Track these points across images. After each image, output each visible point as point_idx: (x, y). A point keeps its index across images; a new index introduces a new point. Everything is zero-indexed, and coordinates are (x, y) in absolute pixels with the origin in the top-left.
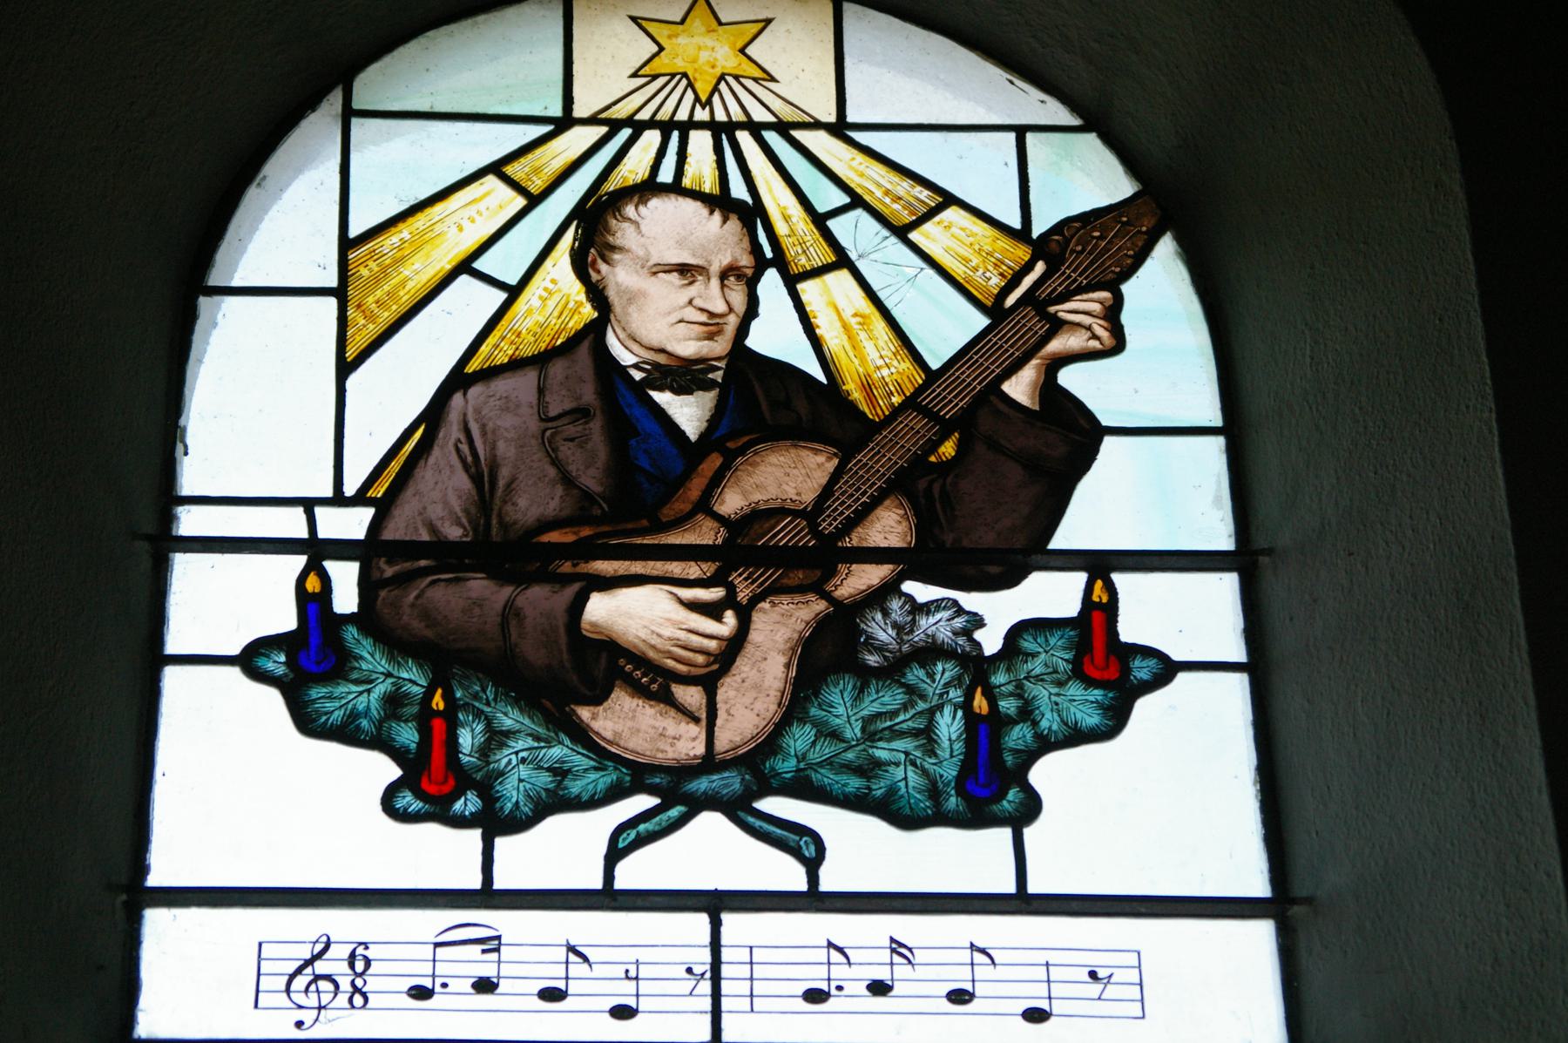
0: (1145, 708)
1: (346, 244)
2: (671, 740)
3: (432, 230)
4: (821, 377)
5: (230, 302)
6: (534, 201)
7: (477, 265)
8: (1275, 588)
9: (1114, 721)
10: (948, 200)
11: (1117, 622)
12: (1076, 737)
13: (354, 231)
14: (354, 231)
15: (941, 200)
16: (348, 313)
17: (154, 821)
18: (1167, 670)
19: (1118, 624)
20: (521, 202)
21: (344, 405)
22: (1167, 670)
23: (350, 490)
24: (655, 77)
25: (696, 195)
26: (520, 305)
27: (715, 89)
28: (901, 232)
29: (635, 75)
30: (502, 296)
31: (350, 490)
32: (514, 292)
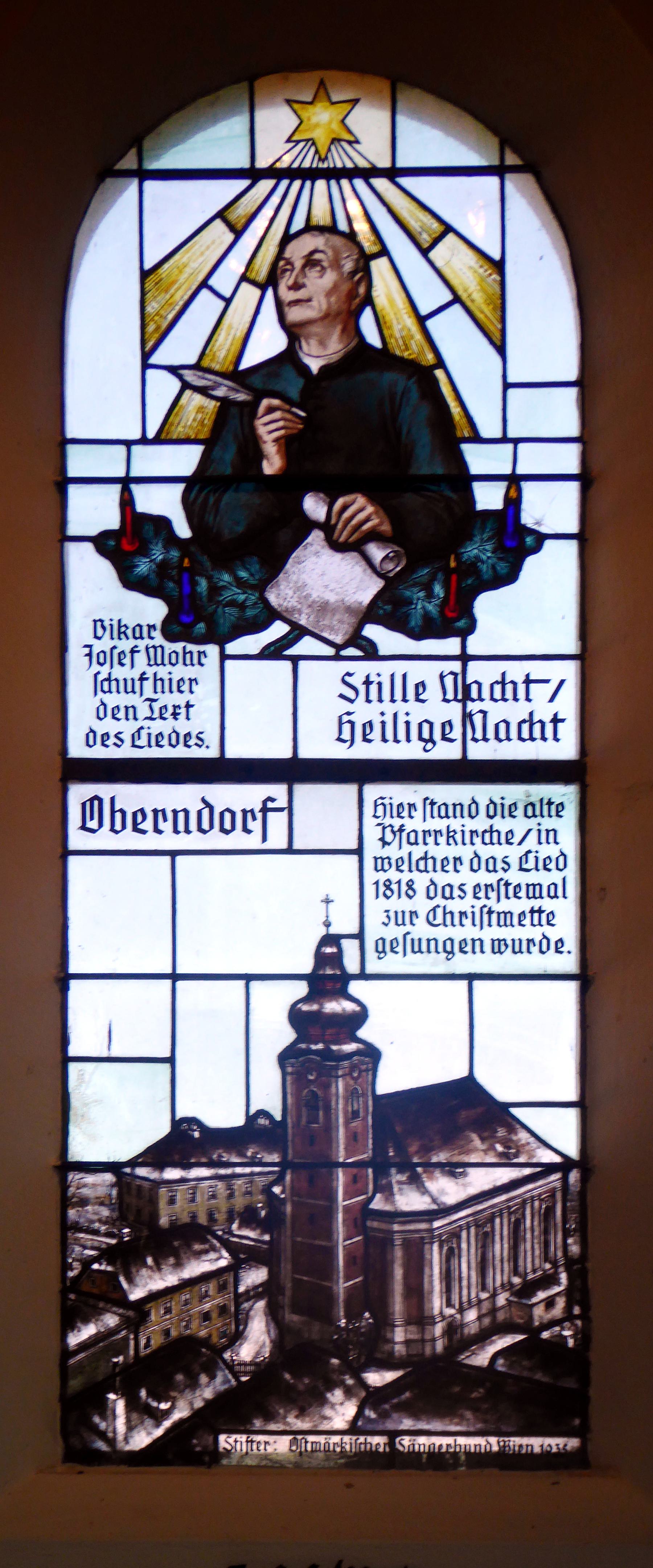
0: (531, 563)
1: (145, 275)
6: (238, 233)
24: (298, 142)
27: (329, 150)
29: (289, 140)
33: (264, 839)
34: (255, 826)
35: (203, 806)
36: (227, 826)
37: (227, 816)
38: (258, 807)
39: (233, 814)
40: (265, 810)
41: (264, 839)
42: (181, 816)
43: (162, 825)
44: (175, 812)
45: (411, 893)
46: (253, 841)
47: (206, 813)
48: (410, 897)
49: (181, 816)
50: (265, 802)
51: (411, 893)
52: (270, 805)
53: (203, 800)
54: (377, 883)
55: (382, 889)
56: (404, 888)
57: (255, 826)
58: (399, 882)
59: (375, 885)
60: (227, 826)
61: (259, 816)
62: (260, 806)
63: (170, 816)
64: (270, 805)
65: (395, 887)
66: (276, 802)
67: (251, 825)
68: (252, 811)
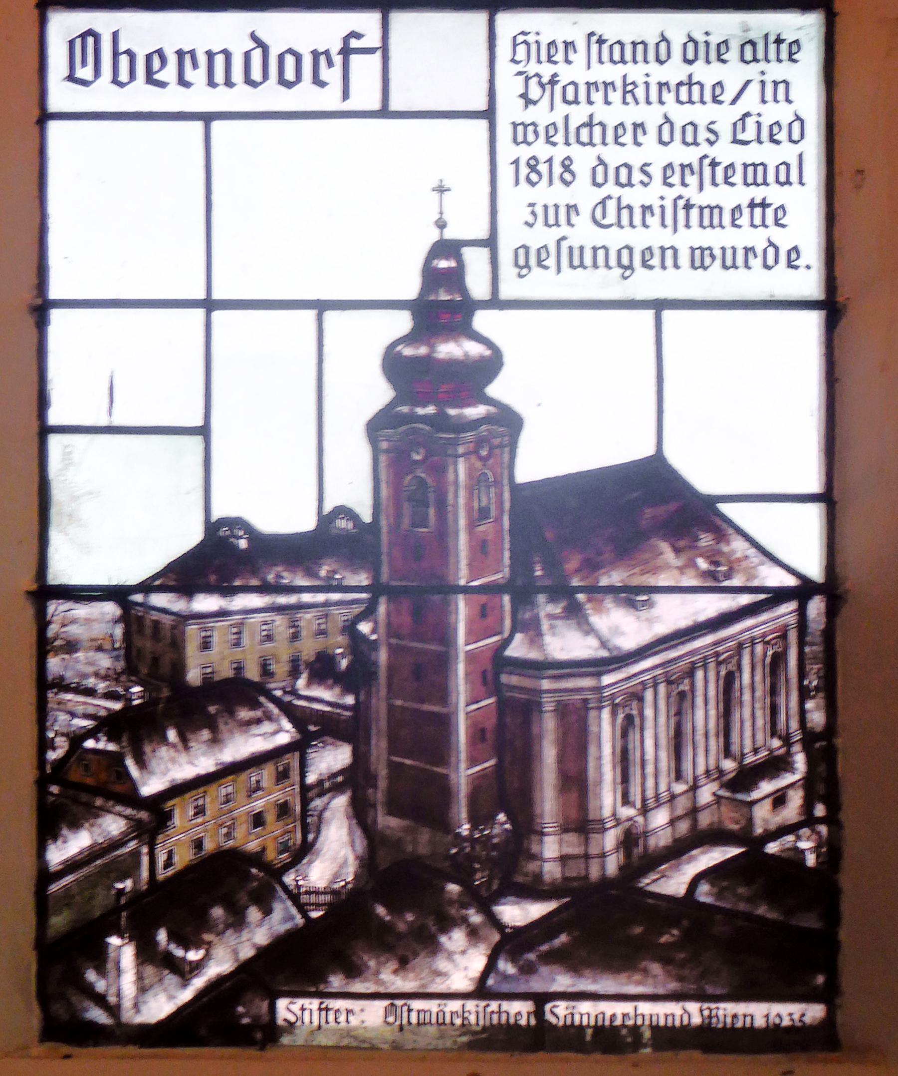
33: (346, 95)
34: (332, 75)
35: (254, 45)
36: (290, 75)
37: (290, 60)
38: (335, 47)
39: (298, 58)
40: (346, 51)
41: (346, 95)
42: (219, 60)
43: (190, 74)
44: (210, 55)
45: (567, 177)
46: (329, 98)
47: (257, 56)
48: (567, 184)
49: (219, 60)
50: (346, 40)
51: (567, 177)
52: (354, 43)
53: (253, 37)
54: (516, 162)
55: (524, 170)
56: (558, 169)
57: (332, 75)
58: (550, 161)
59: (514, 165)
60: (290, 75)
61: (338, 60)
62: (339, 45)
63: (202, 60)
64: (354, 43)
65: (543, 168)
66: (363, 39)
67: (325, 73)
68: (327, 53)
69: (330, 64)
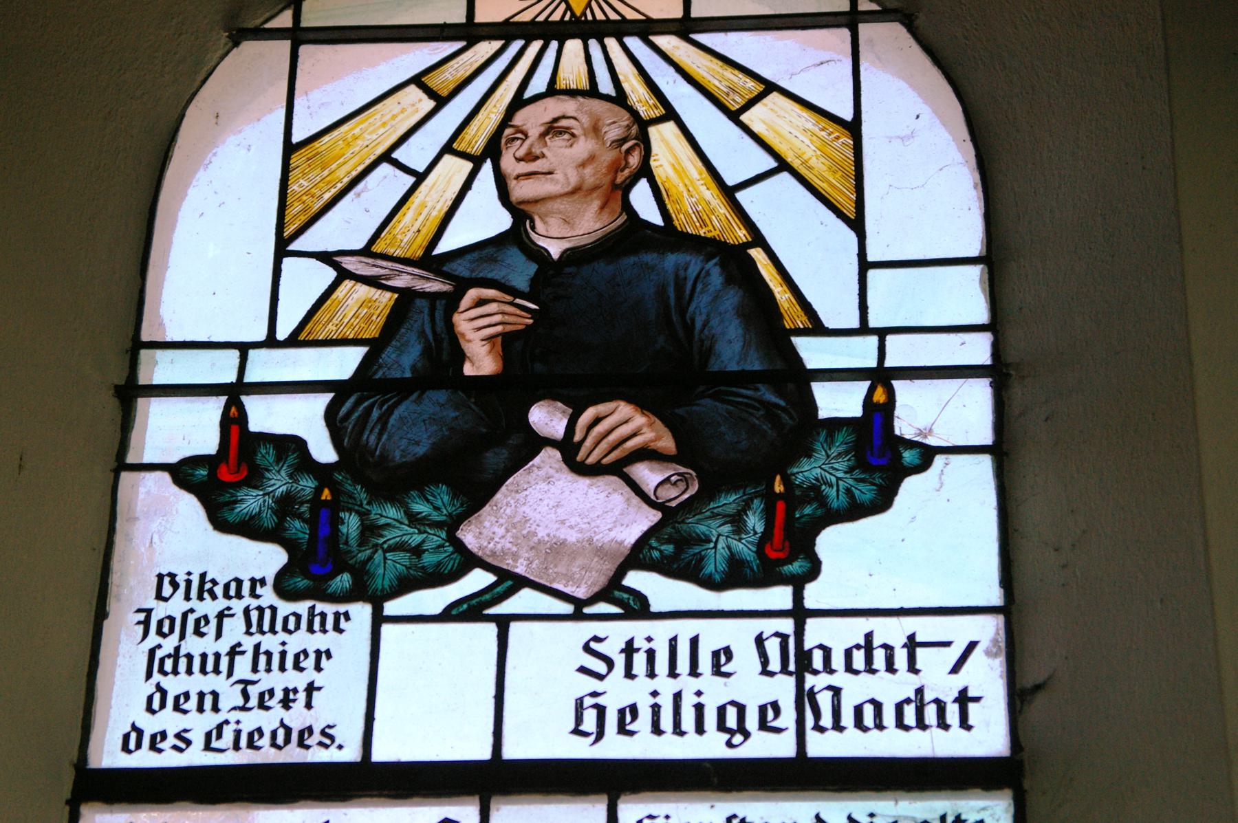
0: (911, 487)
1: (290, 148)
2: (531, 559)
3: (337, 325)
4: (644, 18)
5: (160, 354)
7: (395, 155)
8: (1018, 394)
9: (882, 502)
10: (770, 87)
11: (868, 313)
12: (855, 511)
13: (296, 138)
14: (296, 138)
15: (810, 326)
16: (291, 162)
17: (170, 275)
18: (927, 455)
19: (869, 315)
20: (431, 104)
21: (278, 300)
22: (927, 455)
23: (282, 333)
25: (572, 93)
26: (423, 188)
28: (734, 116)
30: (410, 180)
31: (282, 333)
32: (420, 177)
69: (175, 586)
